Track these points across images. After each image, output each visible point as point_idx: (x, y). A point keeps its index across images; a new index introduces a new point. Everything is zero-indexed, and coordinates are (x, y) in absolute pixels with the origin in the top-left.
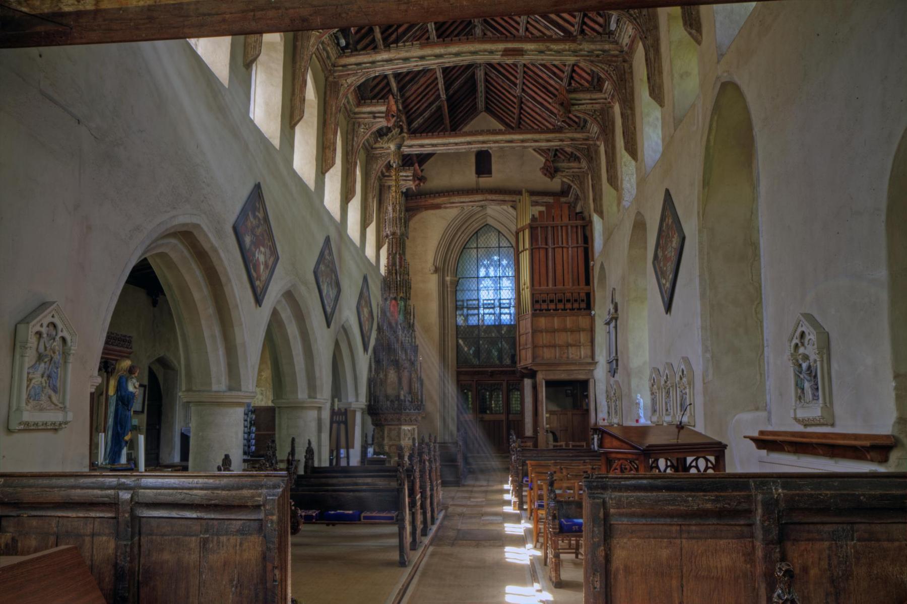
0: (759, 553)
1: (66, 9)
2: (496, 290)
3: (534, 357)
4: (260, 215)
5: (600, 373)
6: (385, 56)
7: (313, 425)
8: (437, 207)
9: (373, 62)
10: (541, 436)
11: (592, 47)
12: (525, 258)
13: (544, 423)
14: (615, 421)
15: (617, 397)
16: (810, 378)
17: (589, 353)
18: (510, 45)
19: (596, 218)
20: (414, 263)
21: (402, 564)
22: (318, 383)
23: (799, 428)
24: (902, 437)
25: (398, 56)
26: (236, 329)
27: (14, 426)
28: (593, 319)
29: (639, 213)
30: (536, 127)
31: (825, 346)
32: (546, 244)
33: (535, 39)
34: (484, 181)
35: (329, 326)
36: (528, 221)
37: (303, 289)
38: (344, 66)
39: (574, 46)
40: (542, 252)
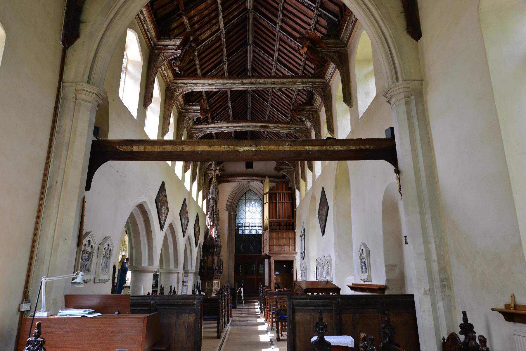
0: (334, 317)
1: (135, 150)
2: (253, 217)
3: (270, 250)
4: (164, 194)
5: (298, 258)
6: (212, 125)
7: (175, 280)
8: (229, 181)
9: (207, 128)
10: (273, 285)
11: (296, 126)
12: (267, 206)
13: (274, 280)
14: (304, 279)
15: (304, 269)
16: (365, 265)
17: (293, 249)
18: (263, 124)
19: (297, 191)
20: (219, 207)
21: (219, 337)
22: (179, 261)
23: (363, 283)
24: (388, 285)
25: (218, 126)
26: (154, 241)
27: (97, 281)
28: (295, 234)
29: (313, 193)
30: (264, 74)
31: (368, 255)
32: (276, 200)
33: (272, 123)
34: (249, 171)
35: (184, 237)
36: (268, 191)
37: (176, 222)
38: (196, 129)
39: (288, 126)
40: (274, 204)
